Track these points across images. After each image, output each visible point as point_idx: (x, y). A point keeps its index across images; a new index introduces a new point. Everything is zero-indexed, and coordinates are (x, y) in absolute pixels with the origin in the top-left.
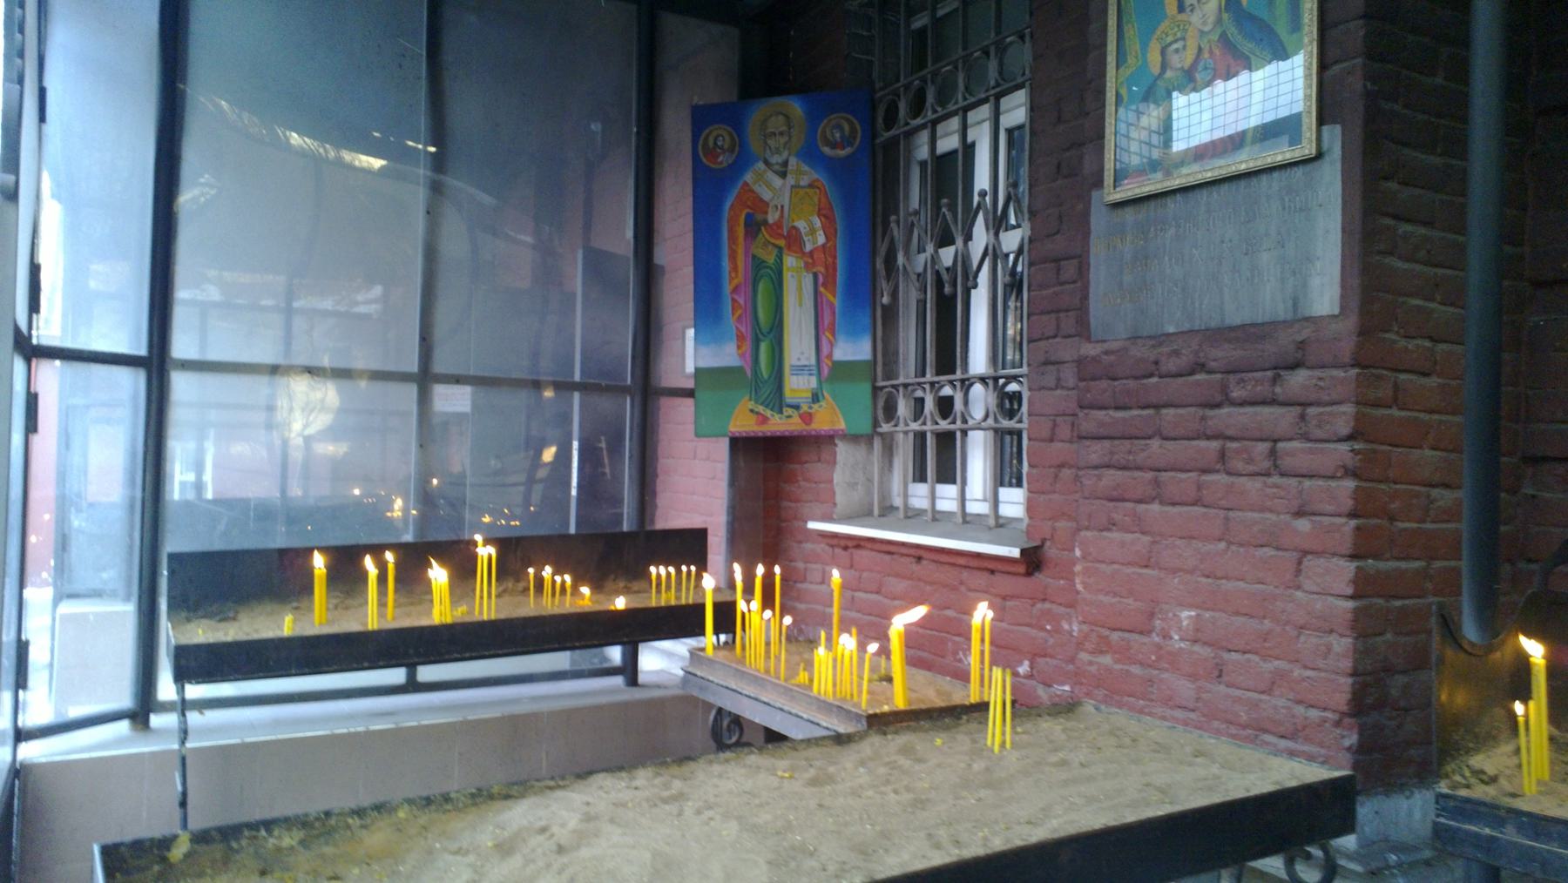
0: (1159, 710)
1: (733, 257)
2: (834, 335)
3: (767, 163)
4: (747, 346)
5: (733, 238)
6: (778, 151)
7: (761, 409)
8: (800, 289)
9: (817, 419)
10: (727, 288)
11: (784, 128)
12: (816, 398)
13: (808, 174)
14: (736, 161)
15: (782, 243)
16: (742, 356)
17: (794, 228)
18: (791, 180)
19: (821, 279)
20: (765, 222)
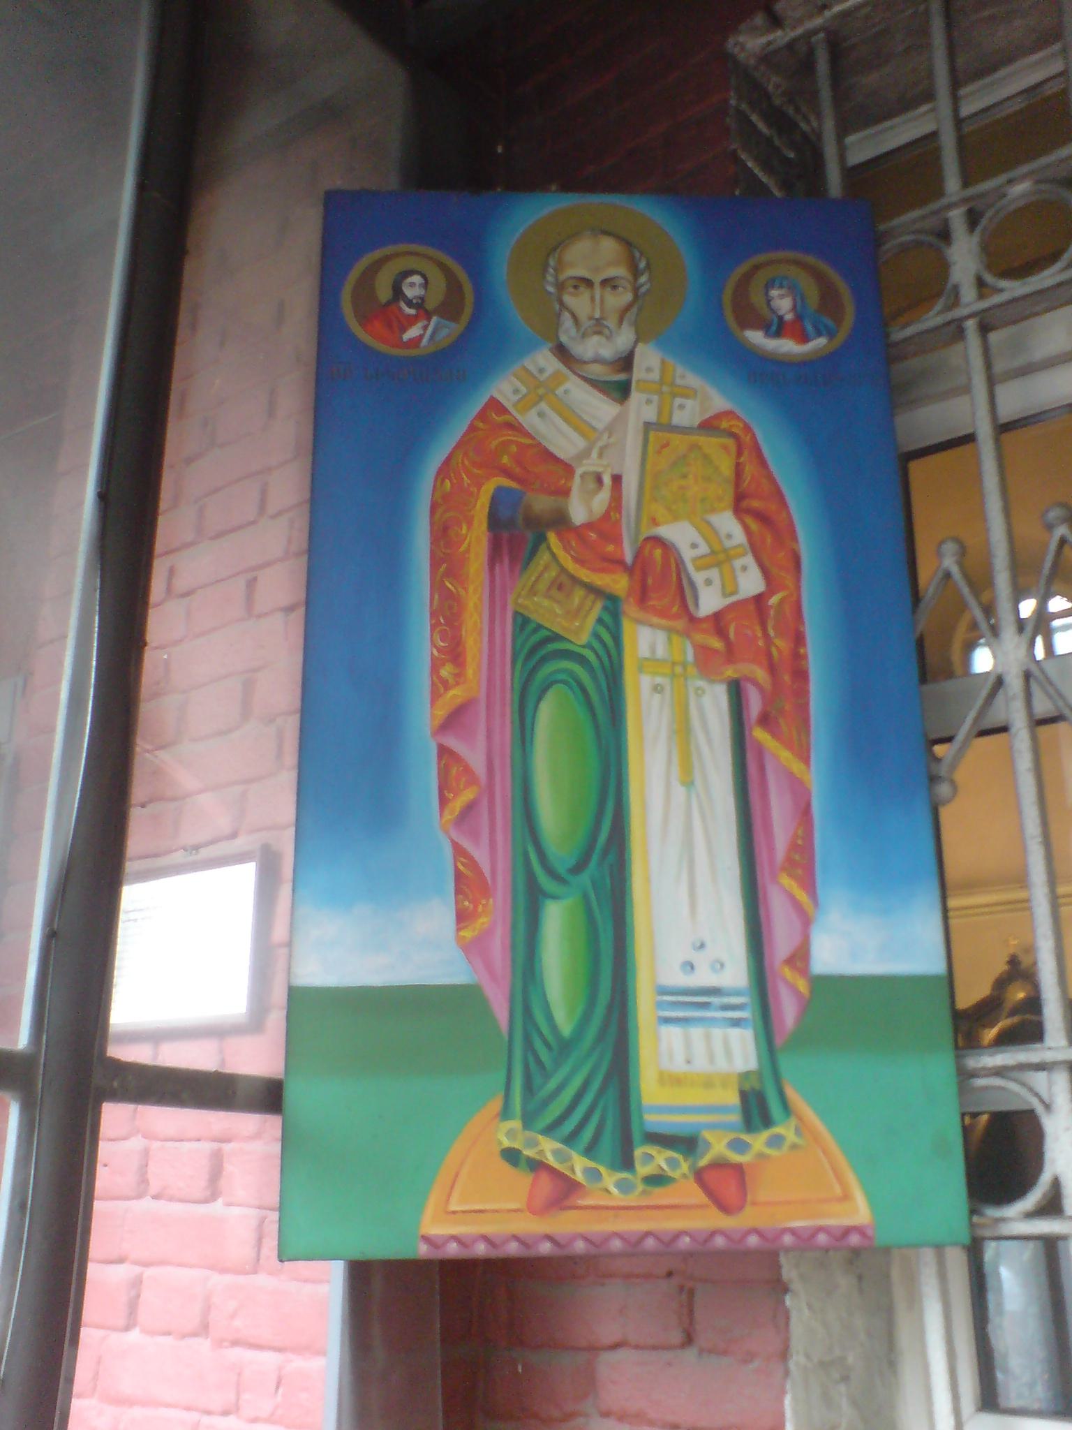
0: (655, 620)
1: (447, 615)
2: (809, 884)
3: (562, 352)
4: (495, 914)
5: (446, 562)
6: (599, 327)
7: (548, 1149)
8: (683, 731)
9: (764, 1190)
10: (422, 716)
11: (620, 271)
12: (756, 1108)
13: (706, 395)
14: (470, 328)
15: (619, 583)
16: (474, 949)
17: (657, 541)
18: (641, 407)
19: (755, 705)
20: (560, 521)
